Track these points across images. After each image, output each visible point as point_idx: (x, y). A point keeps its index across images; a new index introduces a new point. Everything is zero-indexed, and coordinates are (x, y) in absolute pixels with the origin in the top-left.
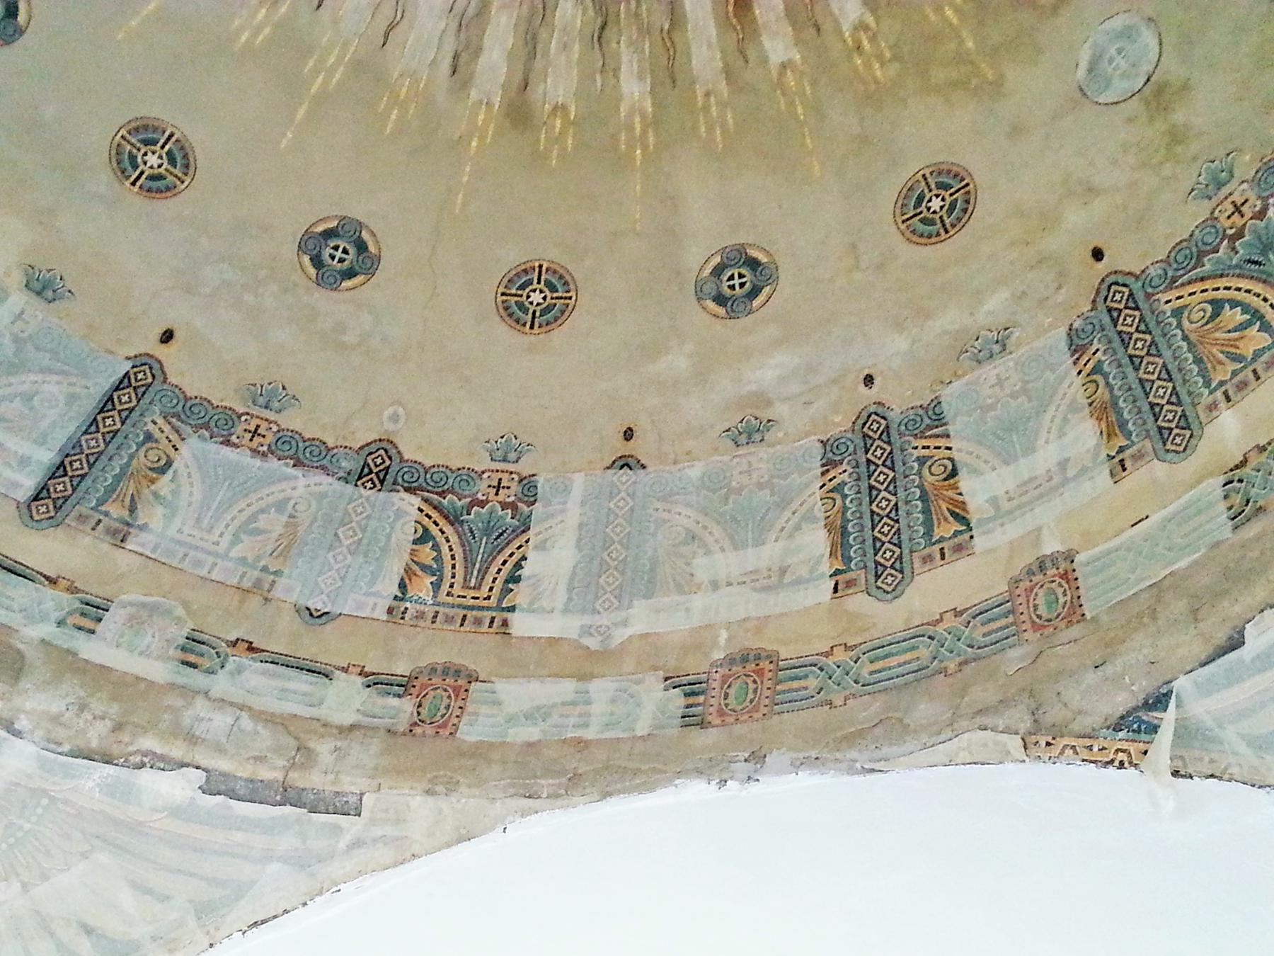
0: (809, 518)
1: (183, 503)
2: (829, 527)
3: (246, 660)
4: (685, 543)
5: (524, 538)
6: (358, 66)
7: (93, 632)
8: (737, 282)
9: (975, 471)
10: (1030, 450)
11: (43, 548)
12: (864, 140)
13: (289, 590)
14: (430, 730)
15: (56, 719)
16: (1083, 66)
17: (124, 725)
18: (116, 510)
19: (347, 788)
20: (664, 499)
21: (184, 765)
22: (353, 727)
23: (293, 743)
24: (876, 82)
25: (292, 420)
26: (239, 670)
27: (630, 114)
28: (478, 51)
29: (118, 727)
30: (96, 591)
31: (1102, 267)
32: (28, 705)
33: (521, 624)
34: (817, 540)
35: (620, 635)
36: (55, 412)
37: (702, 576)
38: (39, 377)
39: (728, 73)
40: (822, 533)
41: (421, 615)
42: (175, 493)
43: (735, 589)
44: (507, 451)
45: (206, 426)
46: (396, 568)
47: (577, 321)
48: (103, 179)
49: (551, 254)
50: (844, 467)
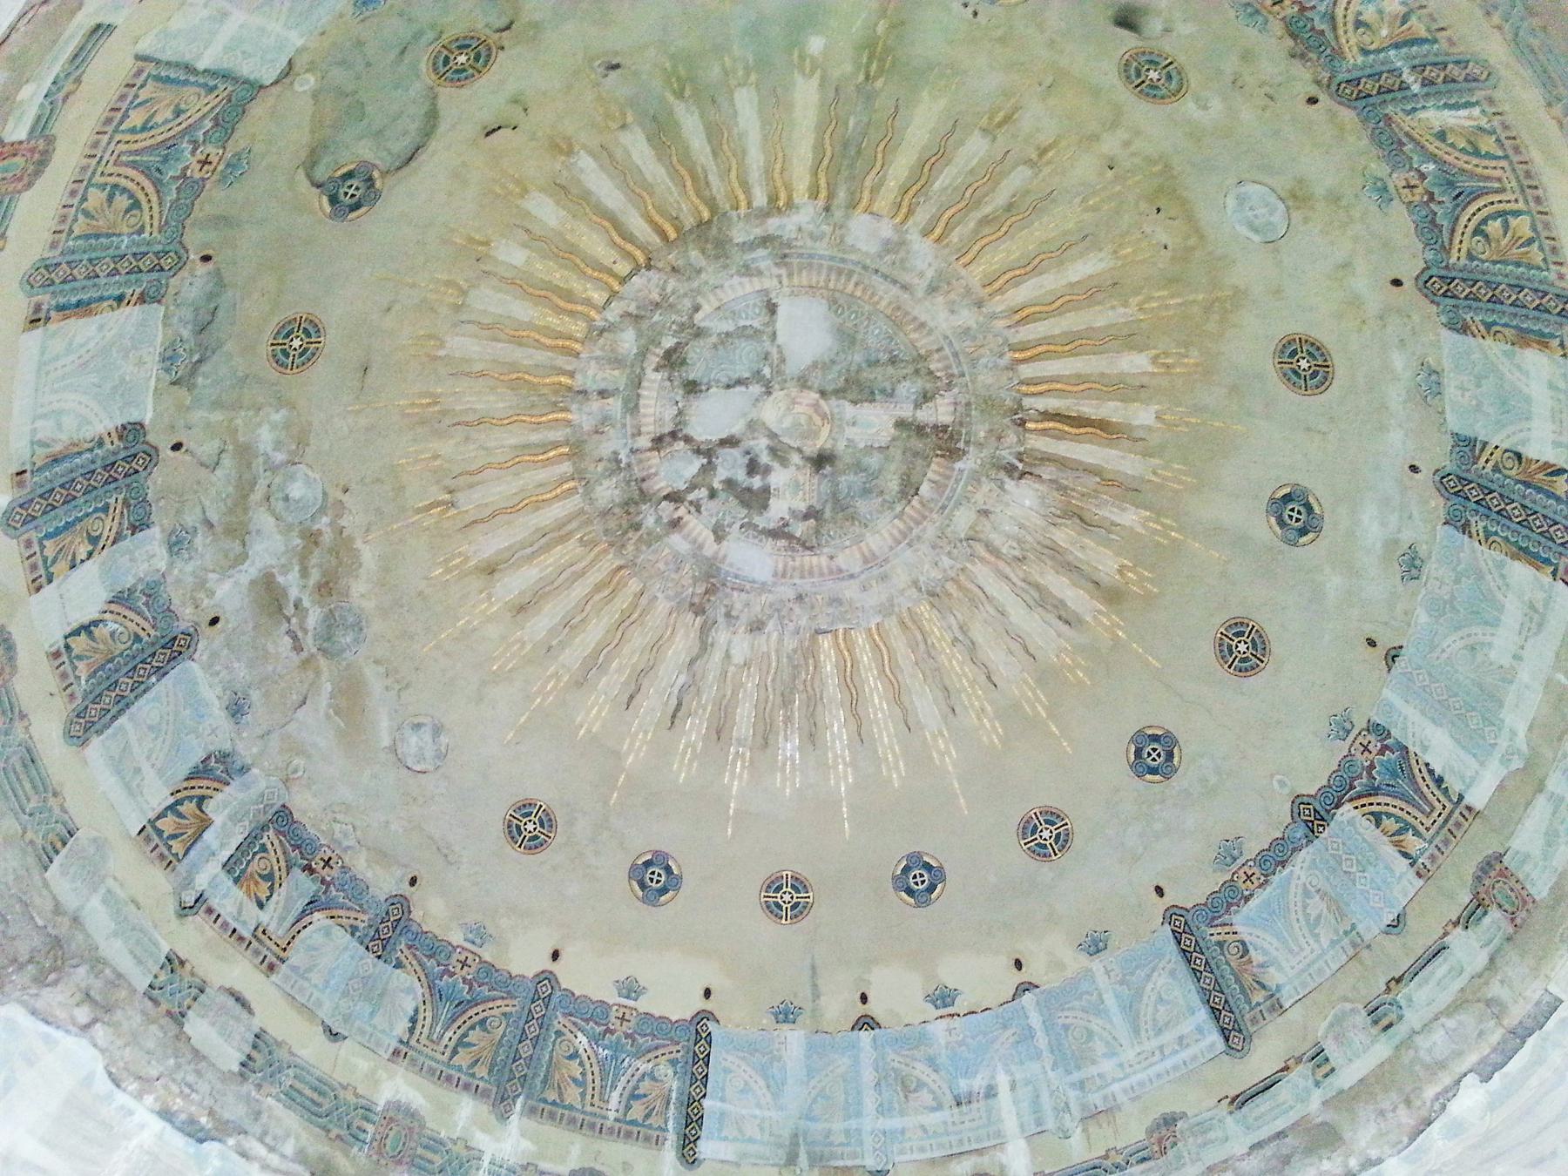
0: (1500, 565)
1: (1275, 953)
2: (1514, 557)
4: (1474, 656)
5: (1412, 755)
6: (1041, 680)
7: (1333, 1070)
8: (1295, 515)
9: (1524, 442)
10: (1528, 400)
11: (1263, 1058)
12: (1234, 389)
13: (1369, 929)
14: (1523, 914)
15: (1381, 1135)
16: (1251, 235)
17: (1407, 1092)
18: (1258, 997)
19: (1536, 996)
20: (1433, 648)
21: (1458, 1082)
22: (1492, 960)
23: (1481, 1005)
24: (1197, 365)
25: (1252, 848)
27: (1144, 526)
28: (1062, 602)
29: (1408, 1102)
30: (1305, 1047)
31: (1408, 284)
32: (1363, 1143)
33: (1478, 797)
34: (1520, 572)
35: (1521, 742)
36: (1173, 988)
37: (1506, 661)
38: (1150, 986)
39: (1146, 454)
40: (1516, 563)
41: (1433, 858)
42: (1265, 953)
43: (1528, 646)
44: (1343, 728)
45: (1230, 905)
46: (1389, 851)
47: (1271, 631)
48: (1045, 871)
49: (1217, 622)
50: (1473, 520)
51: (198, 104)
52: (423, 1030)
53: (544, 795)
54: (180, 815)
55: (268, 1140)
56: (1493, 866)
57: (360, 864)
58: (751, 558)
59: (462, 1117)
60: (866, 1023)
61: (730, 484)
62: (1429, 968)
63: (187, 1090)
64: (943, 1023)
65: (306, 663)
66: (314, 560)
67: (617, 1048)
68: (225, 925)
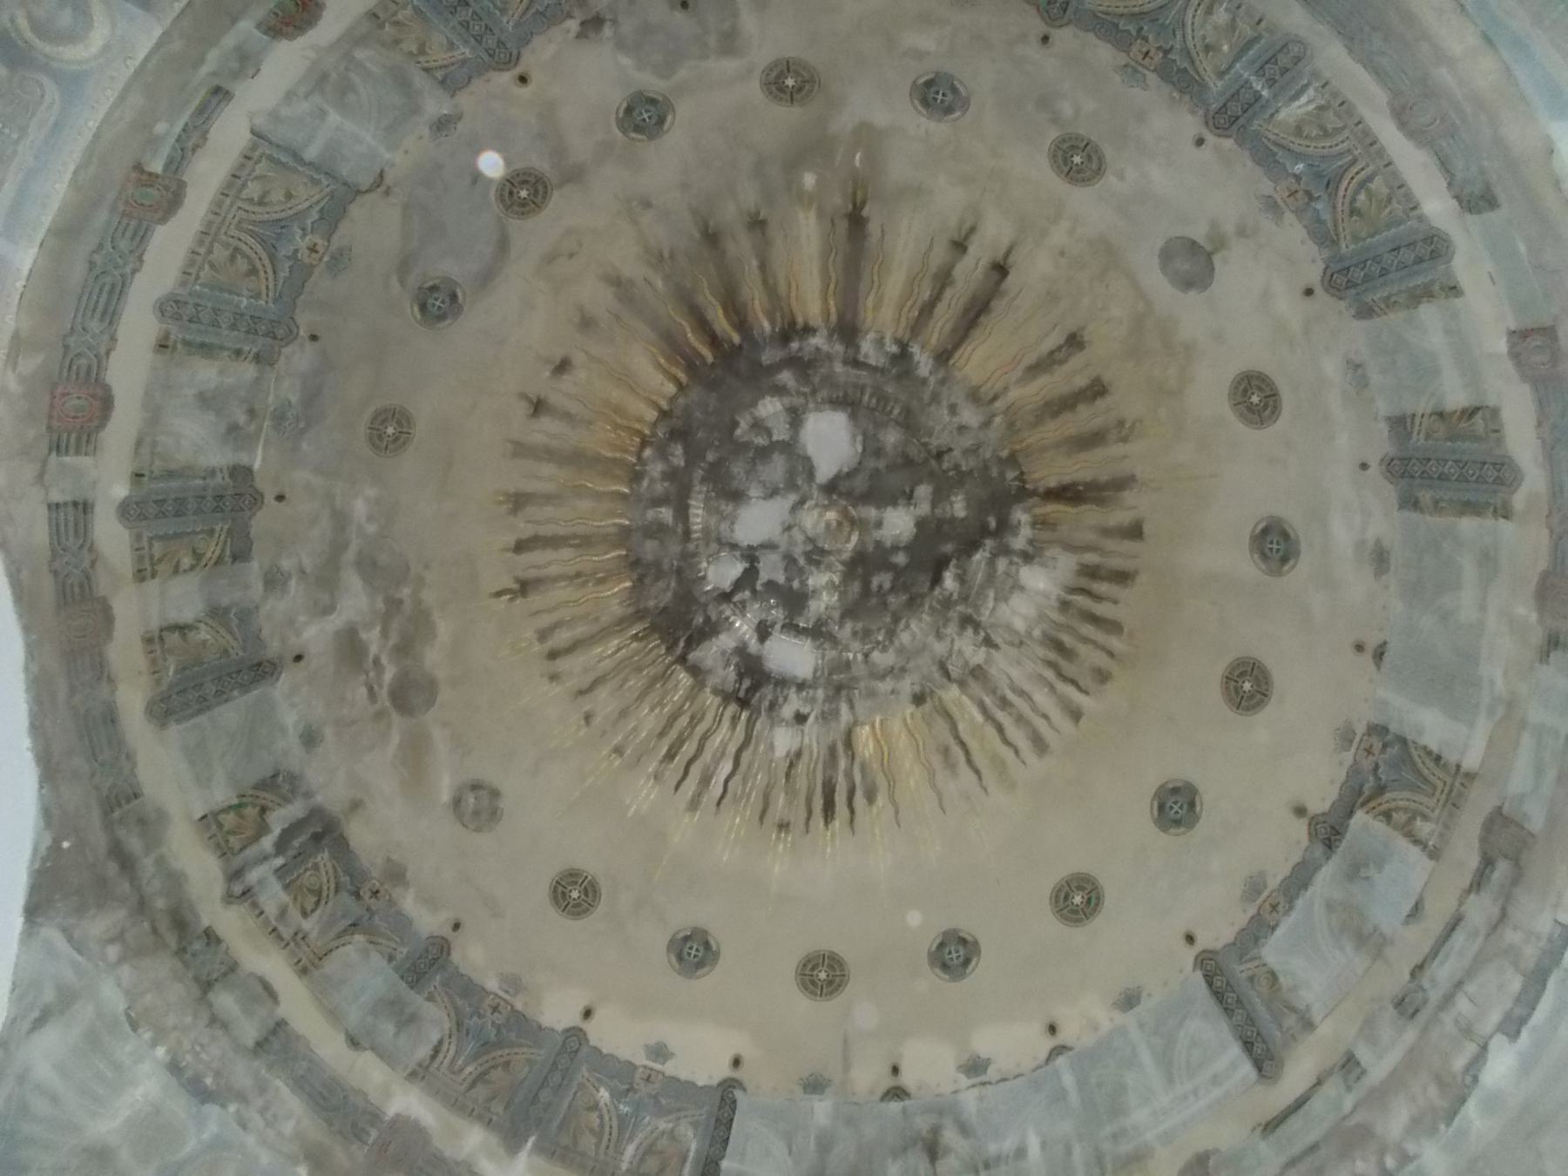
2: (1462, 513)
3: (1428, 973)
11: (1297, 1073)
25: (1273, 882)
26: (1433, 980)
31: (1319, 291)
33: (1471, 761)
36: (1210, 1033)
44: (1346, 737)
46: (1402, 843)
47: (1269, 662)
51: (307, 195)
52: (445, 1058)
53: (590, 864)
54: (242, 817)
55: (269, 1115)
56: (1498, 821)
57: (409, 903)
58: (792, 656)
59: (473, 1141)
60: (897, 1093)
61: (771, 584)
62: (1448, 944)
63: (198, 1048)
64: (975, 1091)
65: (380, 715)
66: (395, 625)
67: (638, 1106)
68: (267, 922)
